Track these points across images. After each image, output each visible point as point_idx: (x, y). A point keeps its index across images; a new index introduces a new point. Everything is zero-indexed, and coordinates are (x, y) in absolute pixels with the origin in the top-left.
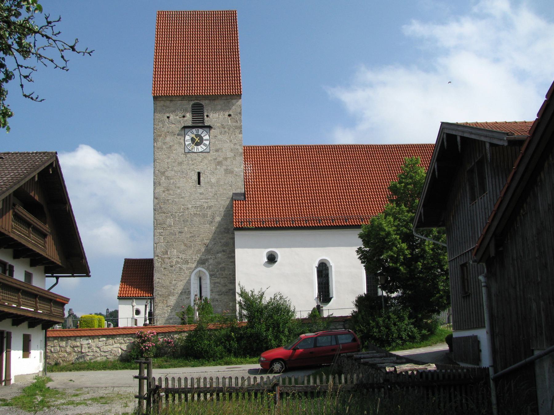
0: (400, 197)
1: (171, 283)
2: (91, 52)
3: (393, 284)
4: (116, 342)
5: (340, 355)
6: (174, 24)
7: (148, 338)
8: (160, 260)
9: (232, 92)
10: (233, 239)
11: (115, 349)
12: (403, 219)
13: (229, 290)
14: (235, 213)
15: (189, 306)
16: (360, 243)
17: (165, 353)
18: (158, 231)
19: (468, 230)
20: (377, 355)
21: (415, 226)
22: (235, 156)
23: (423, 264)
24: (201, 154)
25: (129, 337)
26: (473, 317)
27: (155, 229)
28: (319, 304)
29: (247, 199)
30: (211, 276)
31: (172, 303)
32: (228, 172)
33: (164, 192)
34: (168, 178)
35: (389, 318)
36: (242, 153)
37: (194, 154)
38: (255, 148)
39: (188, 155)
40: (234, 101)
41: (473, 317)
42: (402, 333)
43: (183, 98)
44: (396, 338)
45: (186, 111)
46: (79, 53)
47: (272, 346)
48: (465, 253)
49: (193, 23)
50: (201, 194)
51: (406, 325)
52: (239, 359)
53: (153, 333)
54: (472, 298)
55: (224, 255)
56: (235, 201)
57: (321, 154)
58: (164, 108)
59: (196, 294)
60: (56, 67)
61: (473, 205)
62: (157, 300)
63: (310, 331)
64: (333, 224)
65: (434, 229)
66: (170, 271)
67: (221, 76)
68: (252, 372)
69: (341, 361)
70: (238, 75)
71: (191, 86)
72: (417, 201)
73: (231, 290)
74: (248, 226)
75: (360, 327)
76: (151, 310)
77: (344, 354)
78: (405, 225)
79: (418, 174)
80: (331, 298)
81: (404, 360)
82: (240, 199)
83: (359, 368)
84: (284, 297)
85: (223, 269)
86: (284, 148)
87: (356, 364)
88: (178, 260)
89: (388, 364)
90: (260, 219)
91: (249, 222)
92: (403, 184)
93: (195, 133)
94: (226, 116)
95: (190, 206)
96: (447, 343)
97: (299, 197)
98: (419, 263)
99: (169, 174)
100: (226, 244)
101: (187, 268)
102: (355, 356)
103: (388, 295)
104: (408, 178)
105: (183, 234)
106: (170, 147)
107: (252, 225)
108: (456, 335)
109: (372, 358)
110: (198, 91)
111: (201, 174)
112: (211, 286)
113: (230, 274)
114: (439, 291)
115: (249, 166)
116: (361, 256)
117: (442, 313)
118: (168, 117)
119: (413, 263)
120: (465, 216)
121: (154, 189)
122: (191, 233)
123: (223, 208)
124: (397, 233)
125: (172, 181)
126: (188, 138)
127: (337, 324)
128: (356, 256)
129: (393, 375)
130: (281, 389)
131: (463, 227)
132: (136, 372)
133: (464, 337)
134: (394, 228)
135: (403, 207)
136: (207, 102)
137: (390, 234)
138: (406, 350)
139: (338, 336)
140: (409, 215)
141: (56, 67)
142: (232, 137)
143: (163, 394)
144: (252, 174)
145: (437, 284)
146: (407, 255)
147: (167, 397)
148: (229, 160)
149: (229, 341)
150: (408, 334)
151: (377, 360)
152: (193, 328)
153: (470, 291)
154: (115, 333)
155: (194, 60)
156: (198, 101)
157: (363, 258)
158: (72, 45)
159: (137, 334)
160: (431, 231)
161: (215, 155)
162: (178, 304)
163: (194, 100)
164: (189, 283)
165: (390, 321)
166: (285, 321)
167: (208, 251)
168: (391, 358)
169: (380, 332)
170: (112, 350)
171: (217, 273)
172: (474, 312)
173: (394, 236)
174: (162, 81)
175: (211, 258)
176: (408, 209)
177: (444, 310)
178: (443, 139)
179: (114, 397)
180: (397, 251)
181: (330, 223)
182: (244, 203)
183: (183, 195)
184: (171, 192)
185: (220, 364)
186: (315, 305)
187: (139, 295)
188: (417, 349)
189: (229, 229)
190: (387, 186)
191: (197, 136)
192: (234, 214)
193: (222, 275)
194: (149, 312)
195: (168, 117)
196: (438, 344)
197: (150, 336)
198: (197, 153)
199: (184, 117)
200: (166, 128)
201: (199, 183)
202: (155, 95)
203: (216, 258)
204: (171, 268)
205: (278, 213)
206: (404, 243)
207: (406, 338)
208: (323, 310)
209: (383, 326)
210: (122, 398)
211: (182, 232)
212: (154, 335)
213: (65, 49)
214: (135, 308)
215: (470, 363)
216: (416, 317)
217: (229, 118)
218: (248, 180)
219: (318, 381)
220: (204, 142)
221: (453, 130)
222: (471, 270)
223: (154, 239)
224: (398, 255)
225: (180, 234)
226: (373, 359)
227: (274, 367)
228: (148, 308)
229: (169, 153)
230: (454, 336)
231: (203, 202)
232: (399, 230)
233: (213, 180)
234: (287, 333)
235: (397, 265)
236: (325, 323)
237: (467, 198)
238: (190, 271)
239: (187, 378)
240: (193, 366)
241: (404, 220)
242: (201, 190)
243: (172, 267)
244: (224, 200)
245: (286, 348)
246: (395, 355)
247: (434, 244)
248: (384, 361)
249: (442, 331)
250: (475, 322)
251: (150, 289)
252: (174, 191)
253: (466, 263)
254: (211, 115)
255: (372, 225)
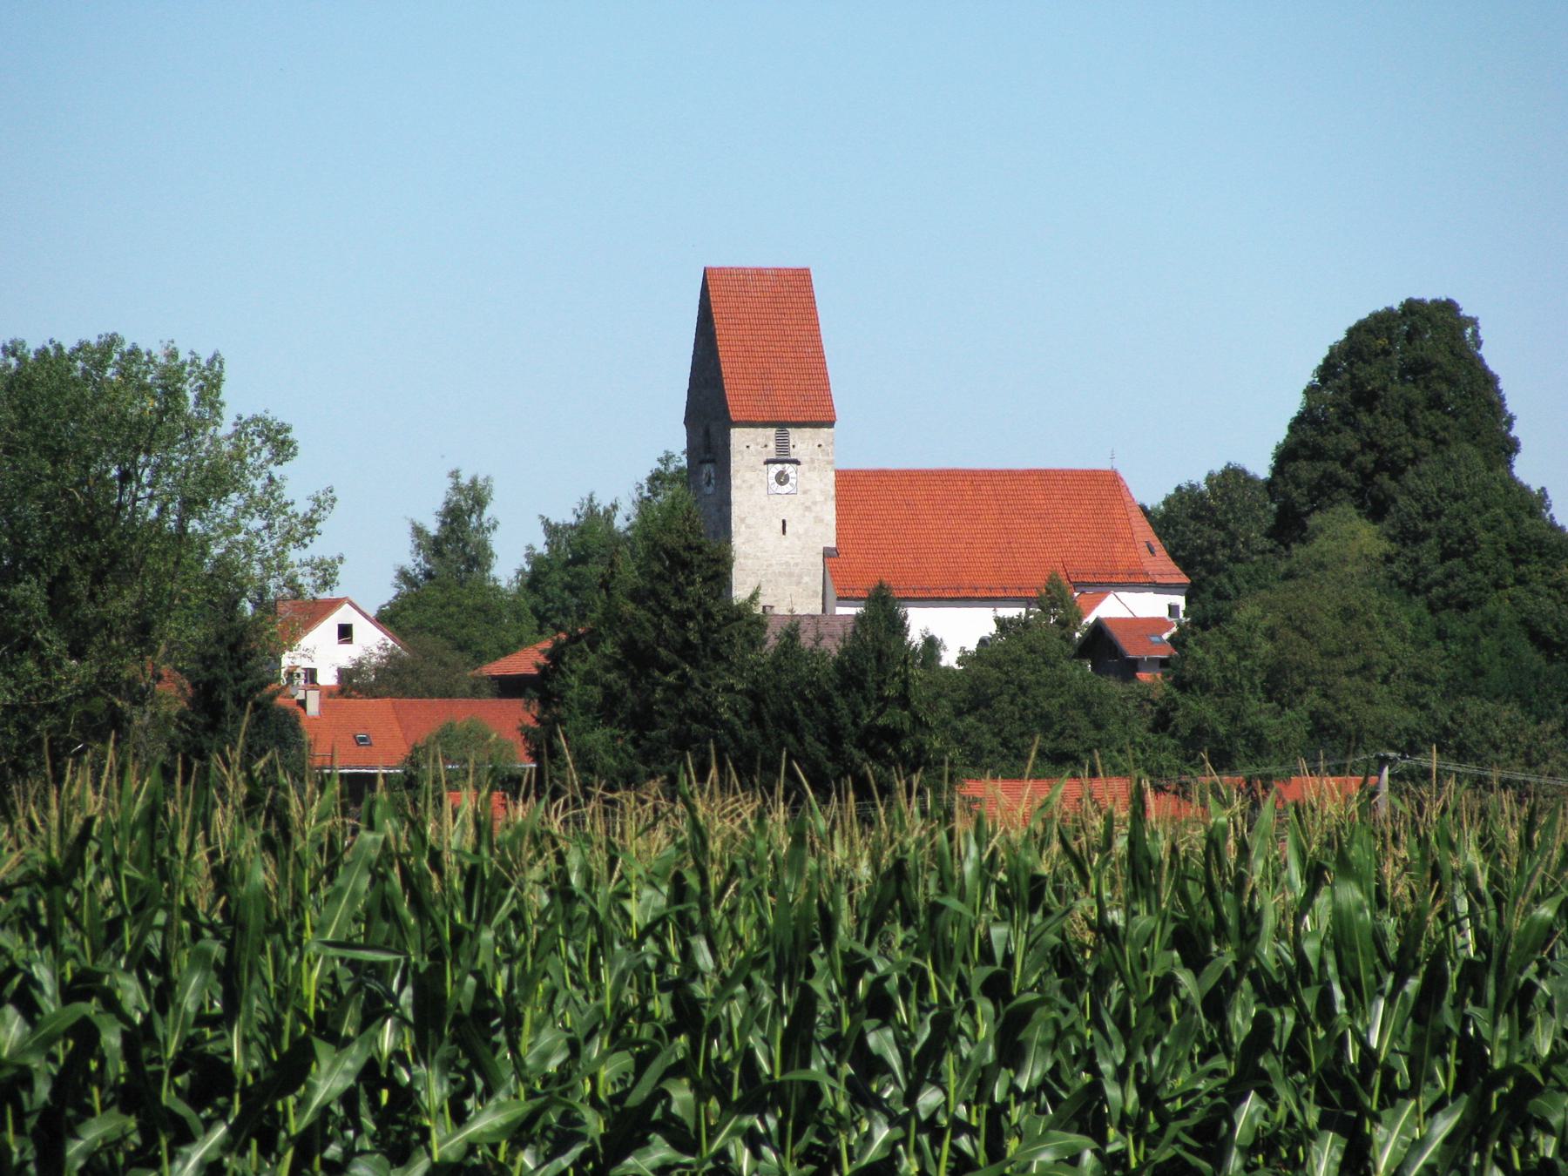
9: (819, 417)
34: (748, 527)
99: (749, 521)
106: (751, 487)
233: (801, 531)
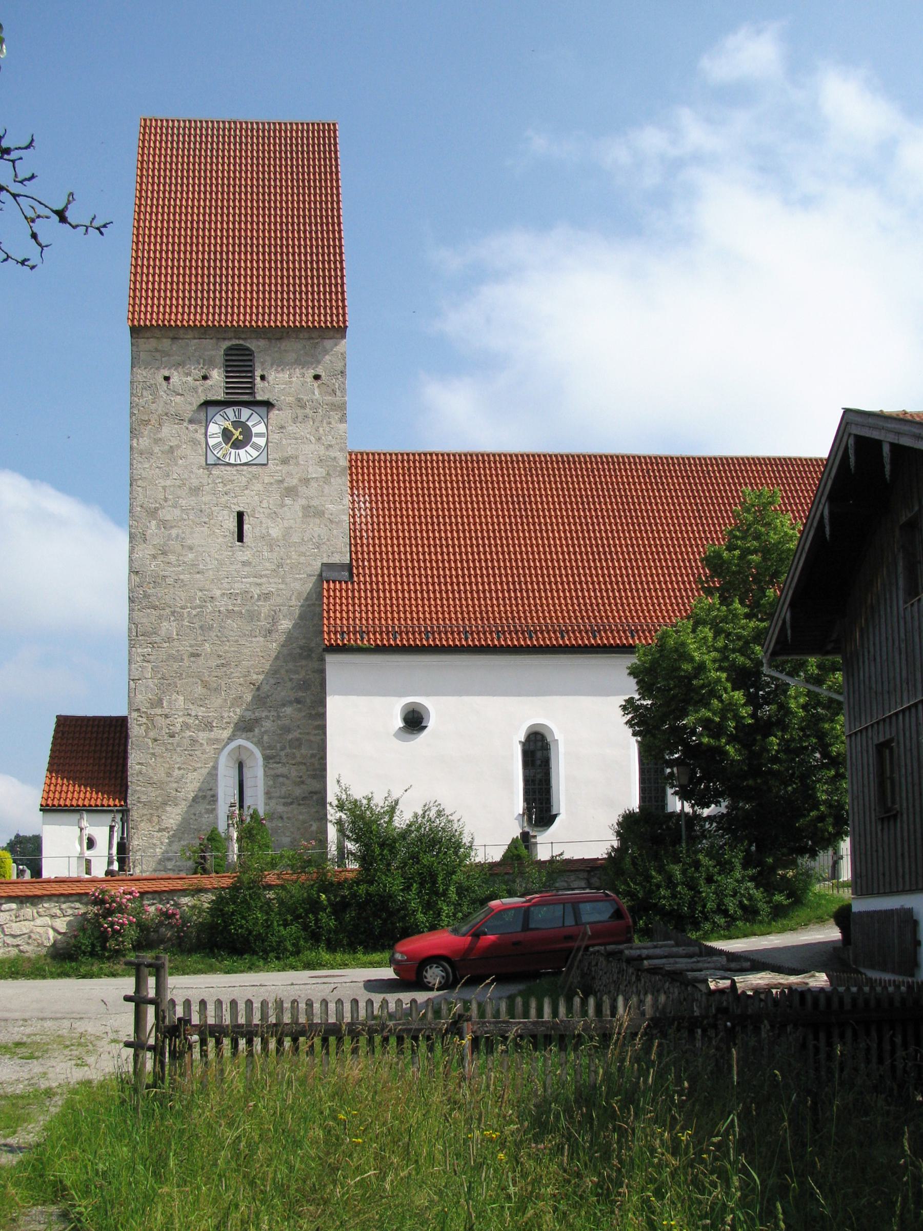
0: (729, 582)
1: (169, 775)
2: (105, 226)
3: (707, 787)
4: (43, 913)
5: (587, 948)
6: (183, 151)
7: (120, 904)
8: (144, 720)
10: (322, 672)
11: (39, 930)
12: (736, 634)
13: (311, 792)
14: (328, 612)
15: (214, 831)
16: (630, 689)
17: (161, 941)
18: (139, 650)
19: (897, 665)
20: (680, 950)
21: (770, 651)
22: (328, 474)
23: (782, 739)
24: (245, 468)
25: (72, 902)
26: (904, 868)
27: (131, 646)
28: (527, 829)
29: (356, 579)
30: (267, 758)
31: (172, 821)
32: (312, 512)
33: (154, 557)
35: (697, 864)
36: (345, 468)
37: (228, 468)
38: (406, 457)
39: (215, 471)
40: (328, 343)
41: (904, 868)
42: (726, 901)
43: (204, 331)
44: (714, 912)
45: (211, 363)
46: (74, 227)
47: (417, 926)
48: (890, 717)
49: (252, 152)
50: (244, 564)
51: (737, 881)
52: (339, 957)
53: (130, 893)
54: (902, 822)
55: (300, 710)
56: (328, 582)
57: (537, 476)
58: (158, 355)
59: (232, 801)
60: (5, 260)
61: (912, 605)
62: (134, 814)
63: (511, 894)
64: (564, 641)
65: (812, 660)
66: (169, 747)
67: (279, 281)
68: (373, 986)
69: (590, 963)
70: (339, 281)
71: (224, 303)
72: (770, 592)
73: (315, 793)
74: (359, 642)
75: (629, 886)
76: (122, 838)
77: (597, 948)
78: (742, 648)
79: (775, 529)
80: (555, 816)
81: (747, 965)
82: (339, 578)
83: (638, 979)
84: (447, 812)
85: (297, 743)
86: (458, 458)
87: (631, 971)
88: (190, 721)
89: (711, 971)
90: (387, 628)
91: (343, 633)
92: (737, 552)
93: (233, 418)
94: (309, 379)
95: (218, 593)
96: (838, 924)
97: (482, 576)
98: (773, 738)
99: (167, 514)
100: (305, 685)
101: (209, 739)
102: (627, 952)
103: (694, 812)
104: (750, 538)
105: (201, 661)
106: (172, 450)
107: (369, 641)
108: (861, 906)
109: (666, 957)
110: (223, 317)
111: (246, 518)
112: (265, 784)
113: (313, 756)
114: (816, 805)
115: (362, 499)
116: (633, 719)
117: (821, 854)
118: (167, 379)
119: (759, 737)
120: (893, 631)
121: (132, 551)
122: (220, 656)
123: (298, 599)
124: (720, 666)
125: (174, 532)
126: (214, 428)
127: (572, 878)
128: (620, 719)
129: (724, 998)
130: (475, 1028)
131: (884, 657)
132: (128, 985)
133: (880, 911)
134: (713, 654)
135: (737, 605)
136: (262, 343)
137: (705, 667)
138: (738, 941)
139: (582, 906)
140: (752, 624)
141: (5, 260)
142: (321, 430)
143: (196, 1037)
144: (369, 520)
145: (814, 789)
146: (744, 718)
147: (203, 1042)
148: (314, 484)
149: (315, 914)
150: (741, 902)
151: (682, 964)
152: (226, 882)
153: (897, 806)
154: (39, 893)
155: (231, 241)
156: (241, 342)
157: (637, 724)
158: (59, 206)
159: (93, 895)
160: (802, 665)
161: (281, 471)
162: (184, 828)
163: (230, 339)
164: (213, 775)
165: (700, 872)
166: (450, 869)
167: (260, 699)
168: (715, 958)
169: (674, 896)
170: (31, 932)
171: (283, 753)
172: (906, 854)
173: (713, 675)
174: (239, 300)
175: (267, 717)
176: (746, 610)
177: (825, 848)
178: (846, 448)
179: (48, 1044)
180: (722, 710)
181: (556, 639)
182: (350, 586)
183: (201, 567)
184: (172, 558)
185: (294, 968)
186: (515, 831)
187: (93, 803)
188: (761, 937)
189: (311, 650)
190: (699, 553)
191: (237, 424)
192: (325, 615)
193: (294, 757)
194: (118, 844)
195: (167, 379)
196: (811, 926)
197: (125, 900)
198: (236, 465)
199: (205, 378)
200: (162, 404)
201: (240, 538)
202: (136, 323)
203: (279, 717)
204: (171, 740)
205: (379, 613)
206: (739, 689)
207: (735, 912)
208: (536, 843)
209: (683, 883)
210: (68, 1047)
211: (198, 655)
212: (134, 897)
213: (39, 217)
214: (87, 832)
215: (893, 972)
216: (760, 863)
217: (316, 384)
218: (358, 534)
219: (562, 1010)
220: (254, 439)
221: (875, 428)
222: (903, 757)
223: (130, 670)
224: (724, 718)
225: (192, 659)
226: (672, 960)
227: (428, 975)
228: (115, 834)
229: (168, 465)
230: (855, 909)
231: (250, 584)
232: (726, 658)
233: (275, 532)
234: (454, 897)
235: (719, 740)
236: (544, 872)
237: (897, 589)
238: (215, 746)
239: (236, 1003)
240: (228, 972)
241: (739, 637)
242: (243, 554)
243: (172, 736)
244: (301, 579)
245: (455, 931)
246: (721, 952)
247: (809, 693)
248: (700, 965)
249: (820, 896)
250: (907, 877)
251: (118, 788)
252: (180, 555)
253: (891, 740)
254: (272, 376)
255: (662, 647)
